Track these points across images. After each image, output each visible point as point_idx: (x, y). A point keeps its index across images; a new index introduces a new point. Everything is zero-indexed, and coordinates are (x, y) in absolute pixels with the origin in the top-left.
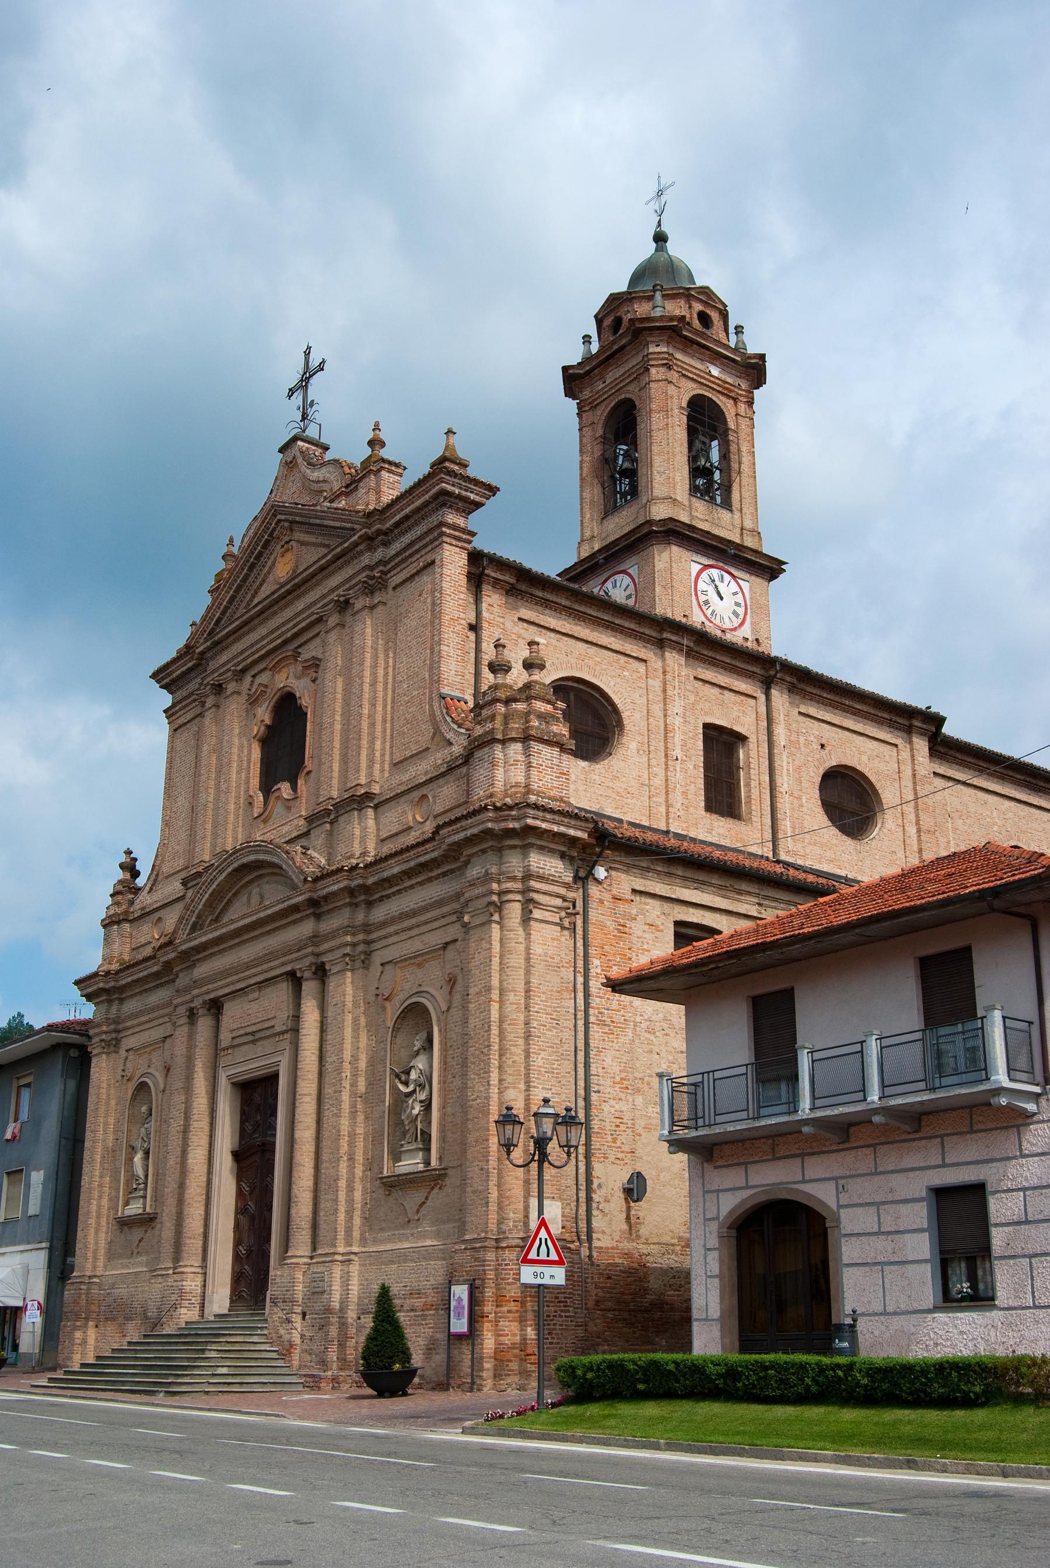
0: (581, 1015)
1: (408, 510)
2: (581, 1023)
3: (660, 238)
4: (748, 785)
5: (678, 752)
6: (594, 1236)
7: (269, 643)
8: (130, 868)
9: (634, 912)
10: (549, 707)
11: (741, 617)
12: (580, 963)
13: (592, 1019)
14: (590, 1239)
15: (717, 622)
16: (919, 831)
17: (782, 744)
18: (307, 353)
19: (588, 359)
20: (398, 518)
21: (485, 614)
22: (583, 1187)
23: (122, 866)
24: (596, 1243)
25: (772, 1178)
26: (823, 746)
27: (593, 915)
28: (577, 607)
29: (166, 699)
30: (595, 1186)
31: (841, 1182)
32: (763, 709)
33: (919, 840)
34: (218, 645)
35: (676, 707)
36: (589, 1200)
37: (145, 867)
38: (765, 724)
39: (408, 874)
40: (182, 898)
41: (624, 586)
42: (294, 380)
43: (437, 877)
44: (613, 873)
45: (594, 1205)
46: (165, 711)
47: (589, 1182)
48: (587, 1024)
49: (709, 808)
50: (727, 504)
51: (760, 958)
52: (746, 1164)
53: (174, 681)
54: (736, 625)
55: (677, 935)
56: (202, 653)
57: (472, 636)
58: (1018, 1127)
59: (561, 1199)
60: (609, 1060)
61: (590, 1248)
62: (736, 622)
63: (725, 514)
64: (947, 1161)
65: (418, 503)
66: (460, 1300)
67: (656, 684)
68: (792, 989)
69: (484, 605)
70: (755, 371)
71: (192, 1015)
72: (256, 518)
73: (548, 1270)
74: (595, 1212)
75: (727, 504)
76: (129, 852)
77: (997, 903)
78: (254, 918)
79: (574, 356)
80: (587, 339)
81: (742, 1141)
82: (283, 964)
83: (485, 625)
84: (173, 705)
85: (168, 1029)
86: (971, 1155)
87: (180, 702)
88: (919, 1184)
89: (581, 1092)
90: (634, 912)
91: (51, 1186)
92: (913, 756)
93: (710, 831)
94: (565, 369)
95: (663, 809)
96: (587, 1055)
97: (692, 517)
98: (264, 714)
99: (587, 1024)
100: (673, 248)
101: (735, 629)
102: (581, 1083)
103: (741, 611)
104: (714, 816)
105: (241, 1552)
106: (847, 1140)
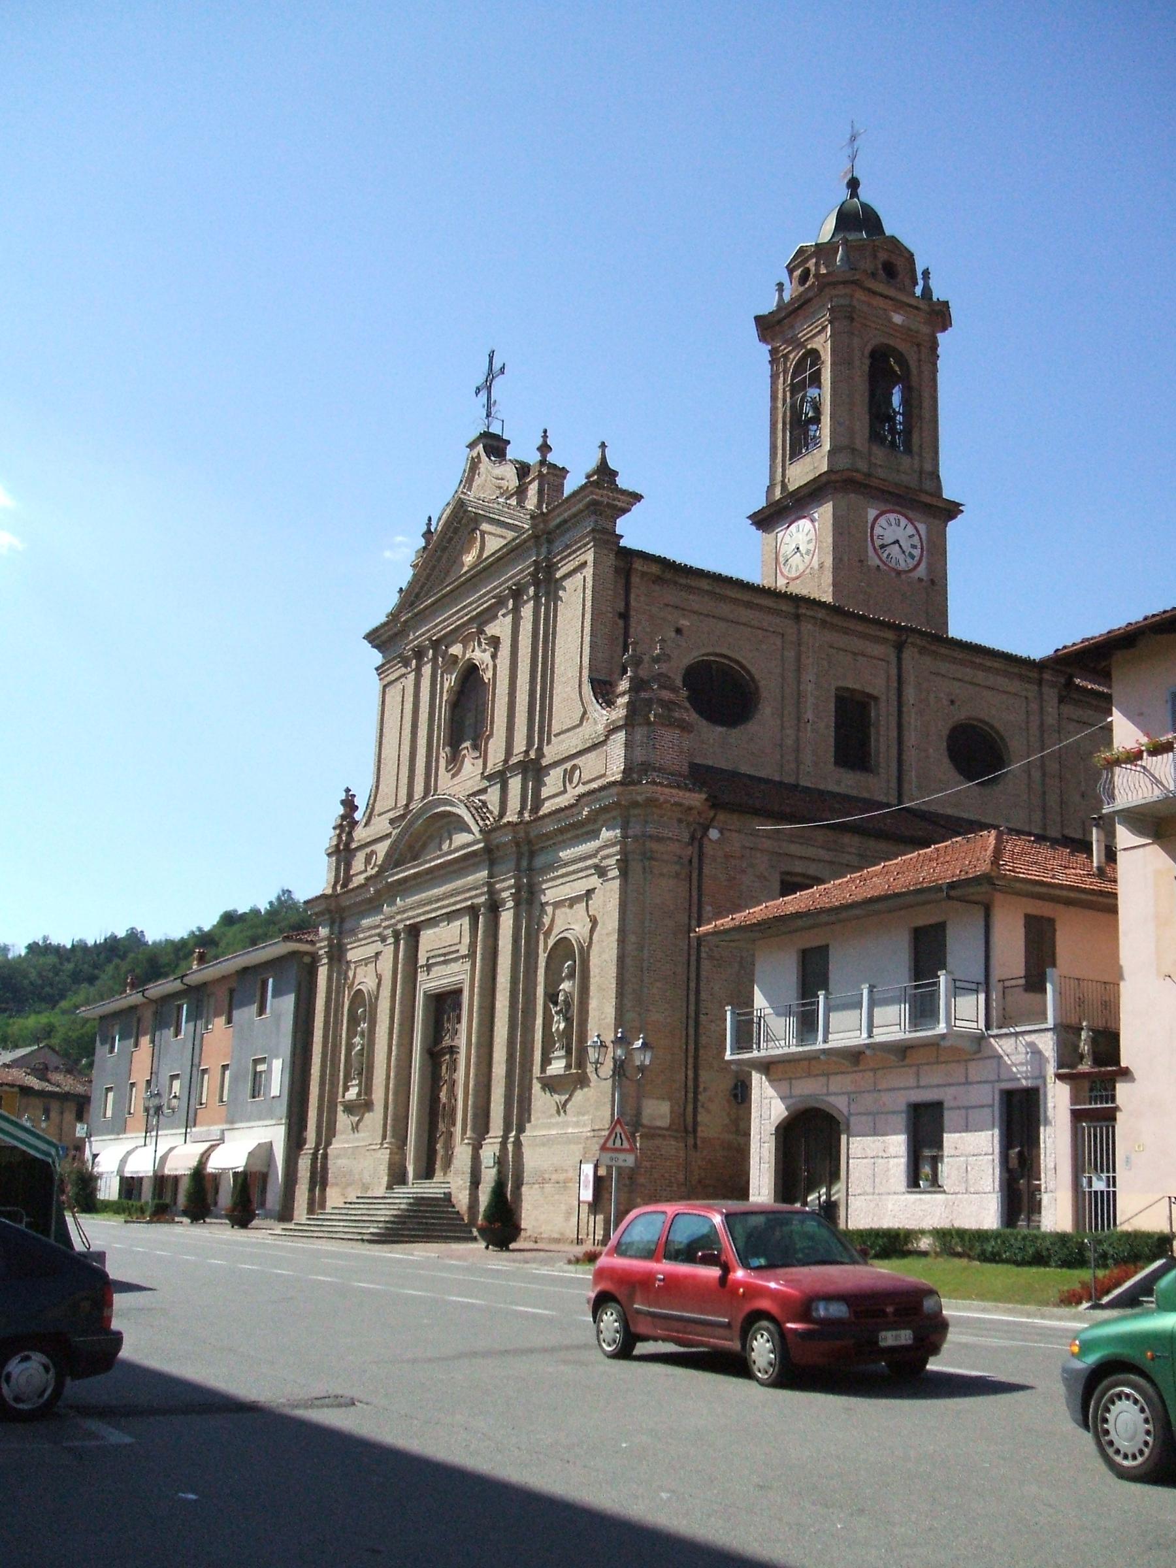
0: (693, 952)
1: (566, 515)
2: (693, 958)
3: (853, 184)
4: (877, 741)
5: (809, 715)
6: (699, 1129)
7: (458, 619)
8: (349, 804)
9: (744, 865)
10: (672, 696)
11: (917, 558)
12: (695, 909)
13: (703, 955)
14: (695, 1131)
15: (893, 564)
16: (1044, 775)
17: (912, 702)
18: (491, 358)
19: (781, 305)
20: (558, 520)
21: (633, 603)
22: (691, 1090)
23: (343, 802)
24: (700, 1134)
25: (809, 1089)
26: (952, 702)
27: (706, 870)
28: (718, 590)
29: (377, 658)
30: (701, 1089)
31: (852, 1096)
32: (894, 671)
33: (1043, 784)
34: (420, 618)
35: (809, 676)
36: (696, 1100)
37: (361, 802)
38: (895, 685)
39: (561, 831)
40: (388, 835)
41: (806, 531)
42: (480, 380)
43: (582, 835)
44: (727, 834)
45: (699, 1104)
46: (377, 669)
47: (696, 1086)
48: (698, 960)
49: (836, 763)
50: (908, 451)
51: (800, 923)
52: (966, 1061)
53: (384, 643)
54: (911, 566)
55: (782, 882)
56: (406, 622)
57: (621, 623)
58: (790, 1079)
59: (670, 1099)
60: (716, 988)
61: (695, 1138)
62: (912, 563)
63: (906, 461)
64: (922, 1083)
65: (574, 510)
66: (587, 1176)
67: (790, 654)
68: (827, 946)
69: (633, 596)
70: (940, 315)
71: (396, 935)
72: (448, 504)
73: (621, 1156)
74: (700, 1110)
75: (908, 451)
76: (348, 790)
77: (952, 893)
78: (442, 860)
79: (768, 305)
80: (780, 286)
81: (789, 1061)
82: (466, 900)
83: (632, 613)
84: (383, 665)
85: (378, 946)
86: (935, 1081)
87: (388, 662)
88: (900, 1100)
89: (692, 1014)
90: (744, 865)
91: (287, 1071)
92: (1041, 708)
93: (839, 783)
94: (758, 319)
95: (793, 766)
96: (698, 984)
97: (871, 464)
98: (450, 681)
99: (698, 960)
100: (866, 194)
101: (911, 571)
102: (692, 1007)
103: (917, 552)
104: (842, 770)
105: (661, 1488)
106: (904, 1058)
